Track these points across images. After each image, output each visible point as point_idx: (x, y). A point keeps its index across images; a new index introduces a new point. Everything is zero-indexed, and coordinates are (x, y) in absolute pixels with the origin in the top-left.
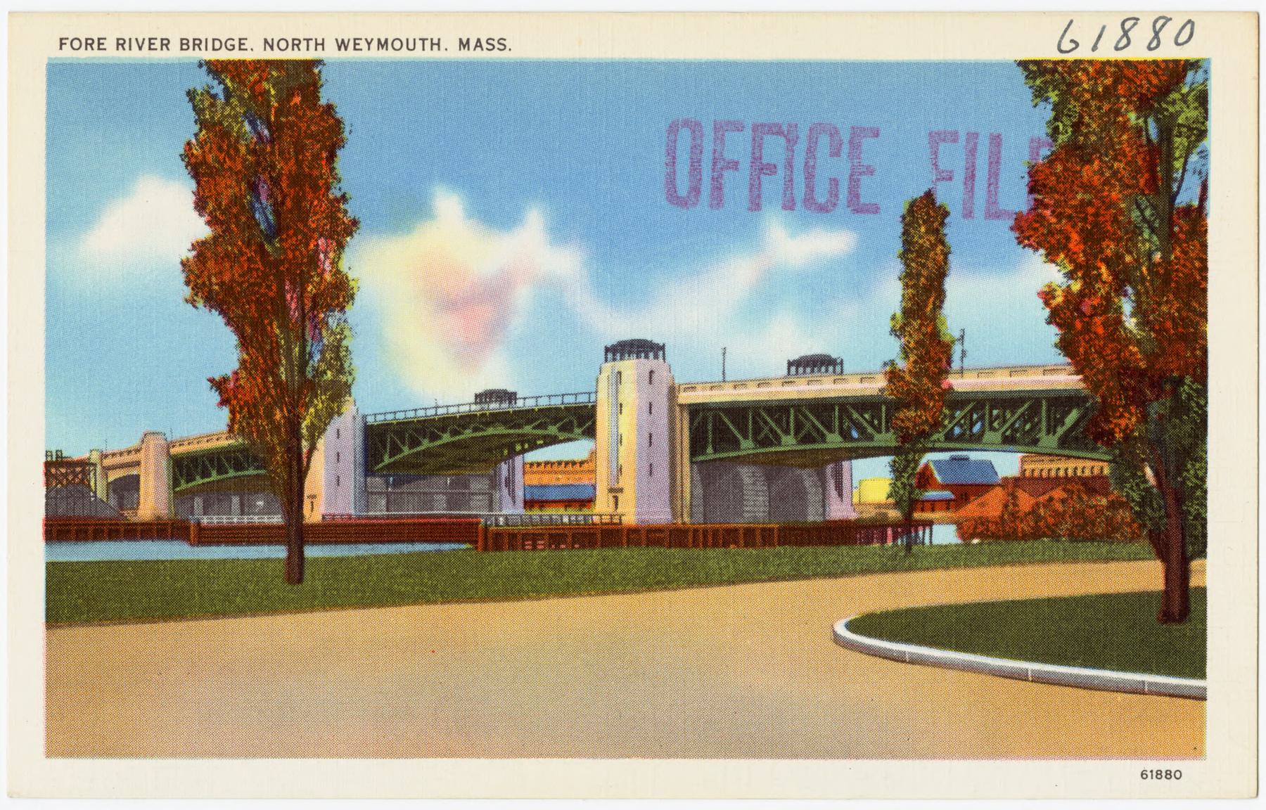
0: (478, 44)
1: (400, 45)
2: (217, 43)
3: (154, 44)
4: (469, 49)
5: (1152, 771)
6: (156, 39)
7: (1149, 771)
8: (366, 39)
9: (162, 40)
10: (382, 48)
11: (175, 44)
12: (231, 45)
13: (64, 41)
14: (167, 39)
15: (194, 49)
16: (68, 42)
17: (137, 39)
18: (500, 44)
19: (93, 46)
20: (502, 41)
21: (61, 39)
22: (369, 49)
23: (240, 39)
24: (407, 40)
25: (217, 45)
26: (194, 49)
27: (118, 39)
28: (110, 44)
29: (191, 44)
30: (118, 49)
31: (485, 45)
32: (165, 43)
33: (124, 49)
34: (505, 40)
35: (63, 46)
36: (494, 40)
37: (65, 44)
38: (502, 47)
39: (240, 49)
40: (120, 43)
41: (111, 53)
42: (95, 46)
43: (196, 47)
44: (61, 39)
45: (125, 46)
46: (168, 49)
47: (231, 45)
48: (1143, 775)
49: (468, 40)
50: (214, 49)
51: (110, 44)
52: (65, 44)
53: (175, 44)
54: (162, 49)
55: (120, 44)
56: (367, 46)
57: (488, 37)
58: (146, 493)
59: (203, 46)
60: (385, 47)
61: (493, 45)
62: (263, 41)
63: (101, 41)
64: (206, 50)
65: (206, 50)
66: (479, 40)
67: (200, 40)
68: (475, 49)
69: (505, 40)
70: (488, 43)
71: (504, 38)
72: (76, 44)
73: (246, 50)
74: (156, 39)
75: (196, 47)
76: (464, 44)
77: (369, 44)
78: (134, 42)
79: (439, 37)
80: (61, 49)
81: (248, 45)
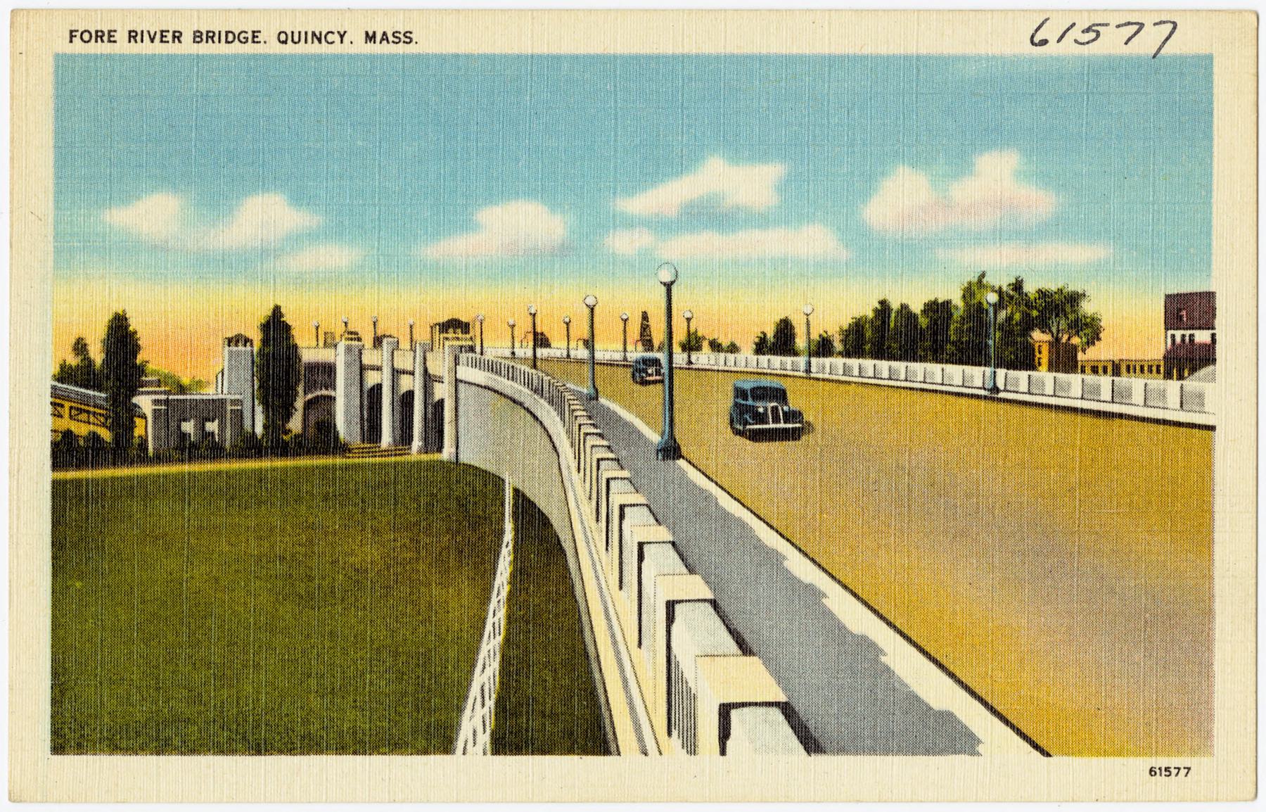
0: (385, 37)
1: (83, 36)
2: (230, 36)
3: (166, 36)
4: (374, 42)
5: (1160, 769)
6: (168, 31)
7: (1157, 768)
8: (338, 32)
9: (175, 32)
10: (370, 42)
11: (187, 37)
12: (244, 38)
13: (74, 34)
14: (179, 32)
15: (207, 42)
16: (78, 34)
17: (149, 32)
18: (407, 37)
19: (103, 38)
20: (408, 35)
21: (71, 32)
22: (342, 42)
23: (254, 32)
24: (293, 33)
25: (230, 37)
26: (207, 42)
27: (130, 32)
28: (121, 36)
29: (204, 37)
30: (130, 42)
31: (391, 38)
32: (177, 36)
33: (213, 42)
34: (411, 33)
35: (74, 38)
36: (400, 33)
37: (75, 36)
38: (408, 40)
39: (254, 42)
40: (132, 36)
41: (122, 46)
42: (105, 38)
43: (210, 40)
44: (71, 32)
45: (214, 39)
46: (180, 42)
47: (244, 38)
48: (1152, 771)
49: (374, 33)
50: (227, 42)
51: (121, 36)
52: (75, 36)
53: (187, 37)
54: (174, 42)
55: (210, 37)
56: (340, 39)
57: (1029, 41)
58: (662, 698)
59: (216, 39)
60: (373, 40)
61: (400, 38)
62: (364, 36)
63: (112, 34)
64: (219, 42)
65: (219, 42)
66: (384, 34)
67: (102, 31)
68: (381, 43)
69: (411, 33)
70: (394, 36)
71: (246, 30)
72: (86, 37)
73: (260, 42)
74: (168, 31)
75: (210, 40)
76: (370, 37)
77: (342, 37)
78: (146, 34)
79: (346, 30)
80: (71, 41)
81: (261, 38)
